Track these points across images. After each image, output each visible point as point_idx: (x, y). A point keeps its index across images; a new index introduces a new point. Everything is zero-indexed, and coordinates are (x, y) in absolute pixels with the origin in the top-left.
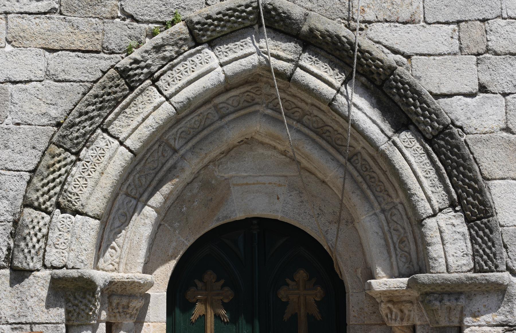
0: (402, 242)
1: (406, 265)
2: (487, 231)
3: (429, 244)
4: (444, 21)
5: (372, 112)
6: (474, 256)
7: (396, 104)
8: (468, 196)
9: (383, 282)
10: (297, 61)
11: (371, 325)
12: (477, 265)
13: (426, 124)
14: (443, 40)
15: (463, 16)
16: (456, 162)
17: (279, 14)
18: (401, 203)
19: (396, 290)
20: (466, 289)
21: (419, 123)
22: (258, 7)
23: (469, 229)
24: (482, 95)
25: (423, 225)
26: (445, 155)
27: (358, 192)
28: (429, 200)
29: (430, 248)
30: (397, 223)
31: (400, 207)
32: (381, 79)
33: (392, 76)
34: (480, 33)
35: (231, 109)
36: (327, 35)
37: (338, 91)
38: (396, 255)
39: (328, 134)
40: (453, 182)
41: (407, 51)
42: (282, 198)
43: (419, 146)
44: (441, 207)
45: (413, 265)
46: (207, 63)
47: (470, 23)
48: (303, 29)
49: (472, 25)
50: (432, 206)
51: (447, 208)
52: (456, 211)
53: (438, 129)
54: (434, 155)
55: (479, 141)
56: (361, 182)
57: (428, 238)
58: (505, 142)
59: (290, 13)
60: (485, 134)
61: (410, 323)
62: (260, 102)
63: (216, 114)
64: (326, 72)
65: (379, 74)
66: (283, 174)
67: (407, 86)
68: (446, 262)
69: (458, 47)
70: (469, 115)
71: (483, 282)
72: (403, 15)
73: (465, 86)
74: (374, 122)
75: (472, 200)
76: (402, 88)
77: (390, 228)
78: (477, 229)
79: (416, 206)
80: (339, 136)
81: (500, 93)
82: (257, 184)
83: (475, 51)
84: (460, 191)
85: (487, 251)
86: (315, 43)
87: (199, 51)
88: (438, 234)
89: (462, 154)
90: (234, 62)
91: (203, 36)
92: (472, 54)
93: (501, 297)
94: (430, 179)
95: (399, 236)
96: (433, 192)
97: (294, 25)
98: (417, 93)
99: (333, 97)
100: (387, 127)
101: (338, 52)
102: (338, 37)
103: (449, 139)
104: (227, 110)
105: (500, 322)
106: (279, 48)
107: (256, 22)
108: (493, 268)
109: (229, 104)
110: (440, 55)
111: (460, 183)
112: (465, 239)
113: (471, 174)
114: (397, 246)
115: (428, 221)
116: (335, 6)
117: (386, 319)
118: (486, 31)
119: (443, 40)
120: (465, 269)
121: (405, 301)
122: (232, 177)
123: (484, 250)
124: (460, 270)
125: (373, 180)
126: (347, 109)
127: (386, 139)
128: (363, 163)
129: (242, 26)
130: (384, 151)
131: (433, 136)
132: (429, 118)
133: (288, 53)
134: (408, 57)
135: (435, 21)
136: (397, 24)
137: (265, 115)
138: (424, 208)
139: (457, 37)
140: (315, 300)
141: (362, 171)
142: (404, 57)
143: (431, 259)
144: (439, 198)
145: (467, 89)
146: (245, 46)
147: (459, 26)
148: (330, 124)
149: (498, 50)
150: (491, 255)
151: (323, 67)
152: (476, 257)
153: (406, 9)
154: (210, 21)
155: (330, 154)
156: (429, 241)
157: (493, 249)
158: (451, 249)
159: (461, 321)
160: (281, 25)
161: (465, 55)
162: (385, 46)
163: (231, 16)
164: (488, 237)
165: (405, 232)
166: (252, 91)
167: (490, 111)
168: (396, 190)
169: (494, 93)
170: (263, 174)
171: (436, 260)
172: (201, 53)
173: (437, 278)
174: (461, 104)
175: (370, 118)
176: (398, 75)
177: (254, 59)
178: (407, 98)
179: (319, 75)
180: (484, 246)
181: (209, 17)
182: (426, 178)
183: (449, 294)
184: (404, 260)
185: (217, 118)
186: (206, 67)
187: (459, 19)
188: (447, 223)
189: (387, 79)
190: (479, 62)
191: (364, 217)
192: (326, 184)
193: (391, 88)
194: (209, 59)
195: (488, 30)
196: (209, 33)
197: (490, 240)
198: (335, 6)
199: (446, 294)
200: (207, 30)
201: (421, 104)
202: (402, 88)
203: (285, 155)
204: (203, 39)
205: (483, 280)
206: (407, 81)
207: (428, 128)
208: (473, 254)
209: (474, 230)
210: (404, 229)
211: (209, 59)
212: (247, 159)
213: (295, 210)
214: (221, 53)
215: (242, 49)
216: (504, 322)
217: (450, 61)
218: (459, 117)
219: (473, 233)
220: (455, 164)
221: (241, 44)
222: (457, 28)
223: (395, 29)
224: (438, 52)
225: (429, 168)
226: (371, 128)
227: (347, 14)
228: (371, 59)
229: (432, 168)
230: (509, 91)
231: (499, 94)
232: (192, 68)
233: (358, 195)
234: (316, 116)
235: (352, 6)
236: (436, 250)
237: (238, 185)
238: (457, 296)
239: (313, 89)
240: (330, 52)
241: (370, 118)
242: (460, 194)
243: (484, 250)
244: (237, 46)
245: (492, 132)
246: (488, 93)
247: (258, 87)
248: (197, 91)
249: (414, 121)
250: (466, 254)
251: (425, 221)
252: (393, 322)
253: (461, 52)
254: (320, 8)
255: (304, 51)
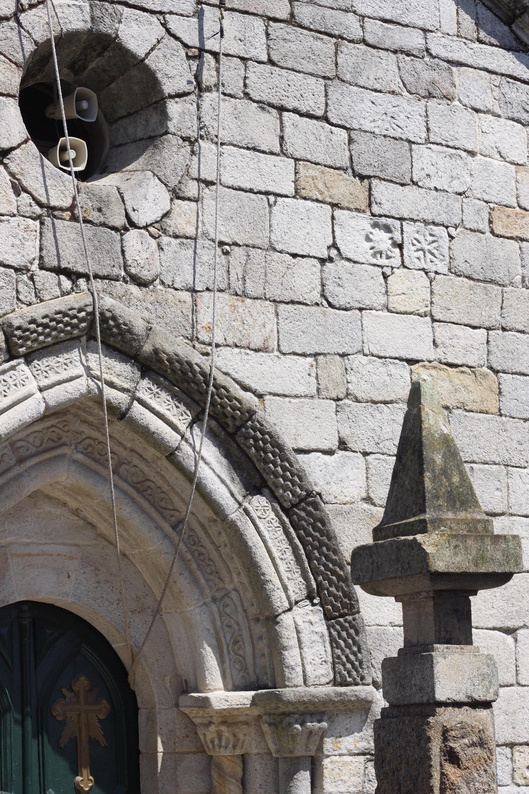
0: (236, 642)
1: (241, 674)
2: (352, 631)
3: (285, 648)
4: (300, 352)
5: (220, 469)
6: (334, 663)
7: (250, 459)
8: (331, 586)
9: (221, 696)
10: (134, 392)
11: (184, 753)
12: (338, 676)
13: (285, 488)
14: (300, 378)
15: (321, 347)
16: (319, 541)
17: (118, 326)
18: (236, 590)
19: (238, 709)
20: (331, 708)
21: (276, 487)
22: (93, 313)
23: (328, 629)
24: (341, 453)
25: (278, 623)
26: (305, 530)
27: (186, 574)
28: (285, 589)
29: (286, 653)
30: (231, 617)
31: (234, 595)
32: (234, 425)
33: (250, 423)
34: (340, 371)
35: (33, 450)
36: (175, 360)
37: (183, 437)
38: (230, 660)
39: (149, 491)
40: (312, 567)
41: (260, 389)
42: (73, 576)
43: (274, 517)
44: (297, 599)
45: (248, 674)
46: (23, 385)
47: (328, 357)
48: (144, 348)
49: (331, 361)
50: (288, 597)
51: (303, 600)
52: (313, 605)
53: (299, 496)
54: (291, 530)
55: (340, 513)
56: (189, 560)
57: (284, 640)
58: (367, 516)
59: (132, 325)
60: (345, 504)
61: (238, 752)
62: (68, 443)
63: (13, 456)
64: (169, 410)
65: (234, 418)
66: (75, 542)
67: (267, 436)
68: (304, 671)
69: (315, 388)
70: (328, 478)
71: (353, 699)
72: (255, 339)
73: (325, 441)
74: (223, 482)
75: (335, 592)
76: (261, 440)
77: (222, 623)
78: (340, 629)
79: (270, 597)
80: (162, 495)
81: (360, 452)
82: (42, 555)
83: (334, 396)
84: (320, 578)
85: (352, 657)
86: (155, 367)
87: (13, 368)
88: (295, 635)
89: (327, 531)
90: (57, 387)
91: (22, 346)
92: (330, 399)
93: (364, 718)
94: (286, 561)
95: (233, 634)
96: (289, 579)
97: (135, 341)
98: (279, 446)
99: (177, 445)
100: (237, 489)
101: (185, 385)
102: (189, 364)
103: (312, 510)
104: (28, 450)
105: (363, 749)
106: (112, 372)
107: (85, 332)
108: (358, 680)
109: (29, 443)
110: (296, 396)
111: (322, 568)
112: (324, 642)
113: (337, 558)
114: (230, 648)
115: (283, 617)
116: (176, 319)
117: (211, 746)
118: (346, 369)
119: (300, 378)
120: (324, 680)
121: (240, 722)
122: (10, 544)
123: (347, 657)
124: (318, 683)
125: (202, 557)
126: (193, 463)
127: (237, 506)
128: (191, 533)
129: (69, 337)
130: (235, 522)
131: (292, 504)
132: (291, 481)
133: (123, 379)
134: (260, 396)
135: (291, 351)
136: (248, 351)
137: (74, 461)
138: (279, 599)
139: (314, 375)
140: (99, 719)
141: (189, 545)
142: (256, 395)
143: (288, 667)
144: (296, 586)
145: (326, 446)
146: (69, 364)
147: (316, 360)
148: (152, 479)
149: (360, 395)
150: (357, 663)
151: (165, 402)
152: (337, 665)
153: (258, 331)
154: (33, 326)
155: (152, 520)
156: (285, 644)
157: (359, 655)
158: (308, 653)
159: (320, 748)
160: (115, 338)
161: (323, 398)
162: (234, 380)
163: (58, 322)
164: (353, 639)
165: (240, 630)
166: (58, 425)
167: (350, 474)
168: (230, 571)
169: (354, 452)
170: (50, 542)
171: (293, 669)
172: (15, 370)
173: (303, 694)
174: (320, 464)
175: (219, 477)
176: (258, 422)
177: (81, 386)
178: (265, 453)
179: (161, 413)
180: (347, 651)
181: (33, 321)
182: (282, 559)
183: (312, 714)
184: (238, 666)
185: (13, 462)
186: (22, 392)
187: (317, 351)
188: (305, 620)
189: (244, 425)
190: (339, 410)
191: (193, 608)
192: (128, 558)
193: (247, 438)
194: (26, 380)
195: (349, 369)
196: (29, 343)
197: (355, 643)
198: (176, 319)
199: (307, 714)
200: (27, 339)
201: (282, 461)
202: (261, 440)
203: (78, 516)
204: (21, 350)
205: (352, 696)
206: (268, 430)
207: (288, 494)
208: (333, 661)
209: (336, 630)
210: (238, 624)
211: (26, 380)
212: (29, 519)
213: (90, 594)
214: (39, 372)
215: (65, 369)
216: (366, 749)
217: (307, 406)
218: (318, 481)
219: (335, 633)
220: (316, 543)
221: (65, 361)
222: (314, 363)
223: (246, 357)
224: (294, 393)
225: (285, 546)
226: (220, 490)
227: (190, 331)
228: (227, 397)
229: (289, 547)
230: (370, 451)
231: (359, 453)
232: (4, 391)
233: (186, 578)
234: (135, 466)
235: (197, 321)
236: (292, 657)
237: (18, 556)
238: (319, 718)
239: (154, 433)
240: (175, 383)
241: (219, 477)
242: (321, 582)
243: (347, 657)
244: (60, 364)
245: (353, 503)
246: (348, 450)
247: (65, 421)
248: (11, 425)
249: (270, 484)
250: (325, 661)
251: (281, 617)
252: (222, 750)
253: (319, 394)
254: (159, 320)
255: (143, 377)
